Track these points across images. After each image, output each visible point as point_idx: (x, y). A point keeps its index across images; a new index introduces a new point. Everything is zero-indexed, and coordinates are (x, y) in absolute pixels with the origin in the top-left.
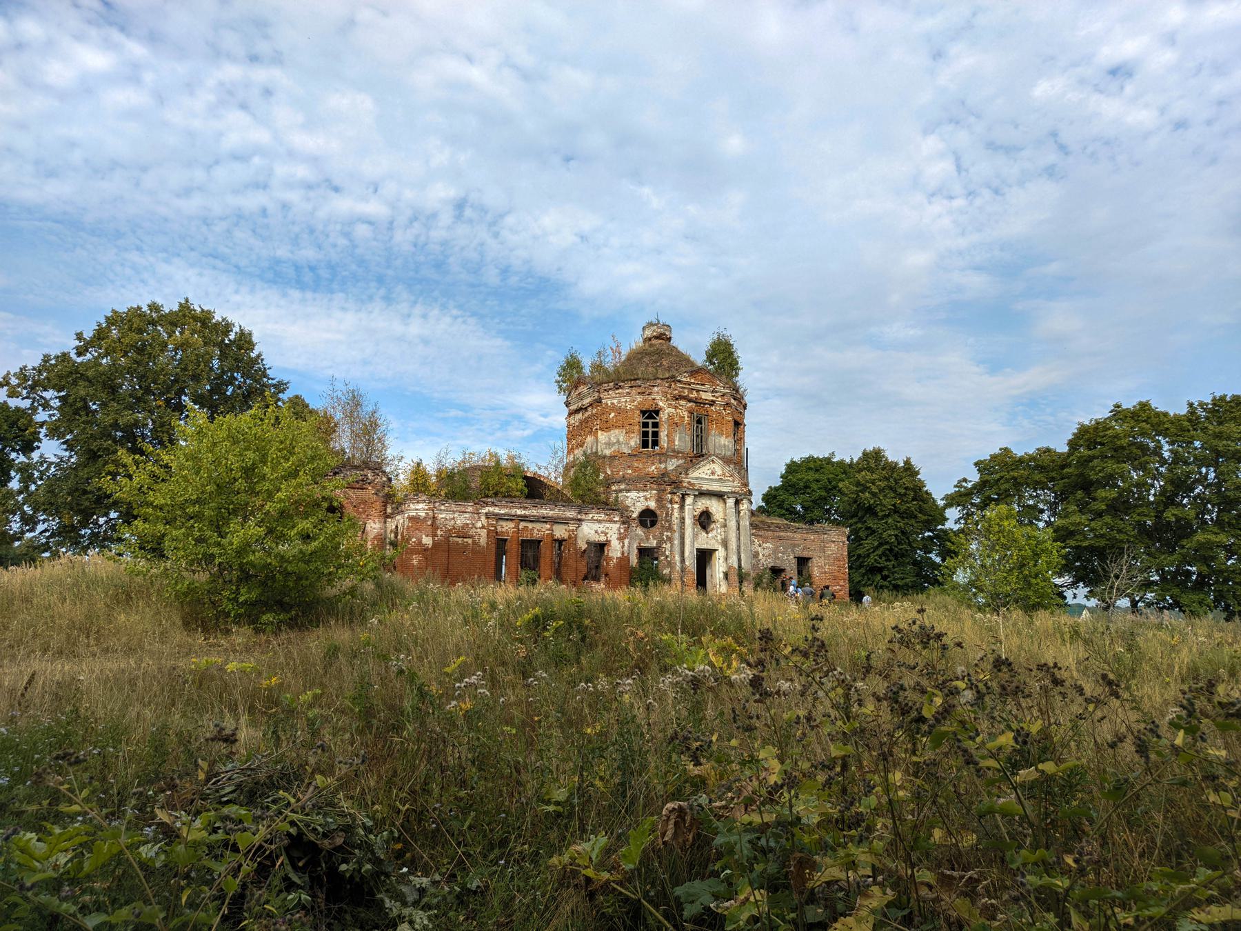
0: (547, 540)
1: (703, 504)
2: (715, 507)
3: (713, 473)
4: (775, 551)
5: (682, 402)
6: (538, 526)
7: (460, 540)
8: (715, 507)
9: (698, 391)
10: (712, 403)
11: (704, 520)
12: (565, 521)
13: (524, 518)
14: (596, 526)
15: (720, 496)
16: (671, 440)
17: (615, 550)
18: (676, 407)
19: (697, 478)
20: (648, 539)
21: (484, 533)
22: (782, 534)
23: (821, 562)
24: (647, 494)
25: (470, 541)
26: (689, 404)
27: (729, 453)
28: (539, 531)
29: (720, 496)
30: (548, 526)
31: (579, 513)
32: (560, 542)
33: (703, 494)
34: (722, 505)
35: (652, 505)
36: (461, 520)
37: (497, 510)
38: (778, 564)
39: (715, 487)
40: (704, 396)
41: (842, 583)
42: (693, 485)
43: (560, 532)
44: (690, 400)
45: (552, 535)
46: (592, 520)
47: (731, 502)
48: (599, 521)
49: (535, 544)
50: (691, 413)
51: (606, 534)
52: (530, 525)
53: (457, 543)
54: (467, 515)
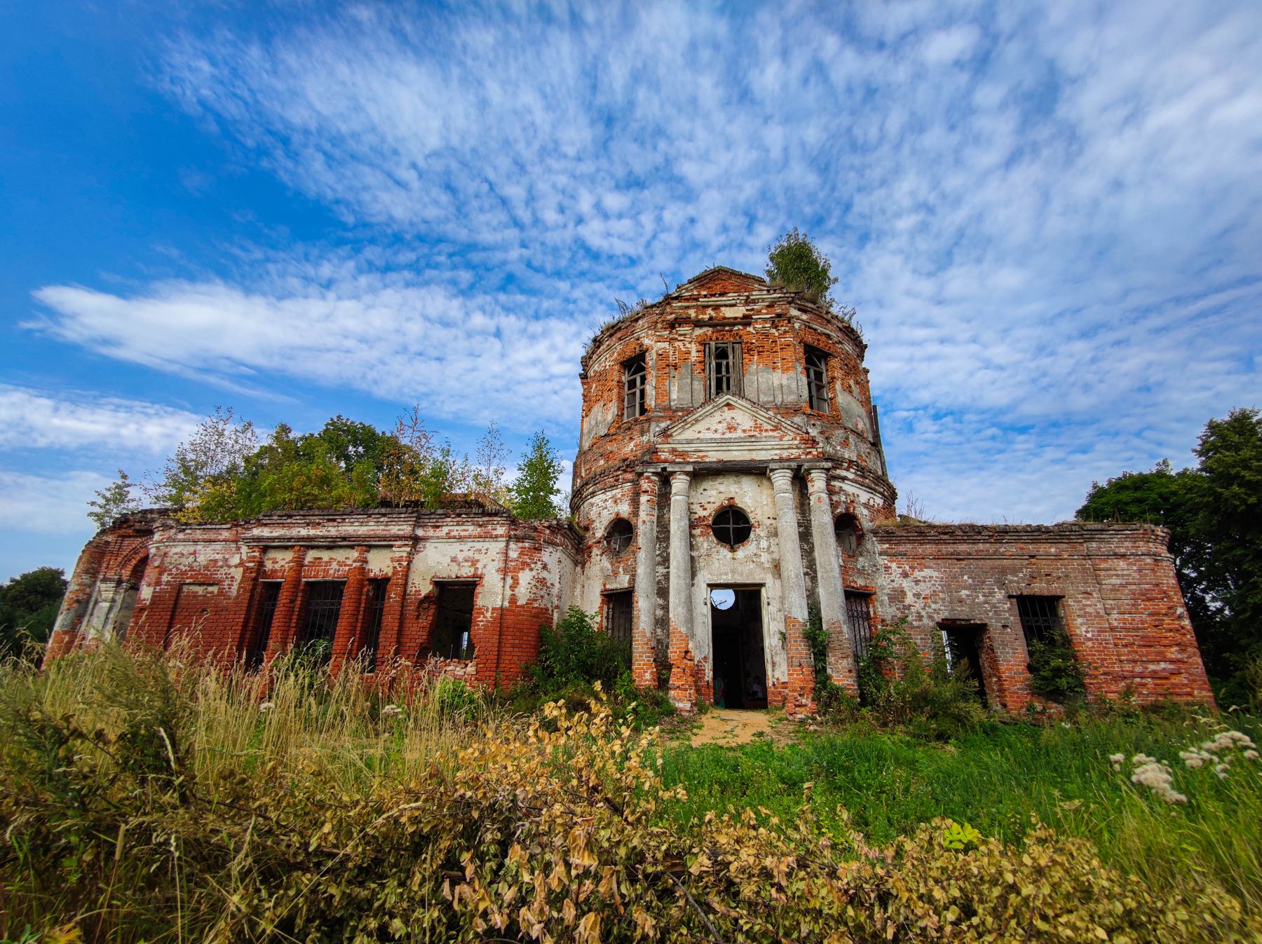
0: (352, 581)
1: (715, 494)
2: (747, 494)
3: (731, 428)
4: (950, 586)
5: (685, 329)
6: (340, 555)
7: (200, 590)
8: (747, 494)
9: (716, 308)
10: (746, 320)
11: (732, 527)
12: (385, 543)
13: (310, 544)
14: (454, 549)
15: (759, 471)
16: (662, 393)
17: (492, 596)
18: (671, 341)
19: (689, 442)
20: (616, 574)
21: (238, 574)
22: (963, 548)
23: (1094, 605)
25: (215, 589)
26: (698, 331)
27: (791, 398)
28: (338, 563)
29: (759, 471)
30: (355, 554)
31: (417, 524)
32: (381, 584)
33: (702, 474)
35: (624, 509)
36: (206, 554)
37: (266, 532)
38: (962, 612)
39: (738, 455)
40: (729, 313)
41: (1173, 653)
42: (683, 454)
43: (380, 563)
44: (698, 324)
45: (362, 570)
46: (449, 536)
47: (782, 479)
48: (461, 539)
49: (334, 589)
50: (703, 343)
51: (474, 563)
52: (325, 555)
53: (195, 595)
54: (218, 546)
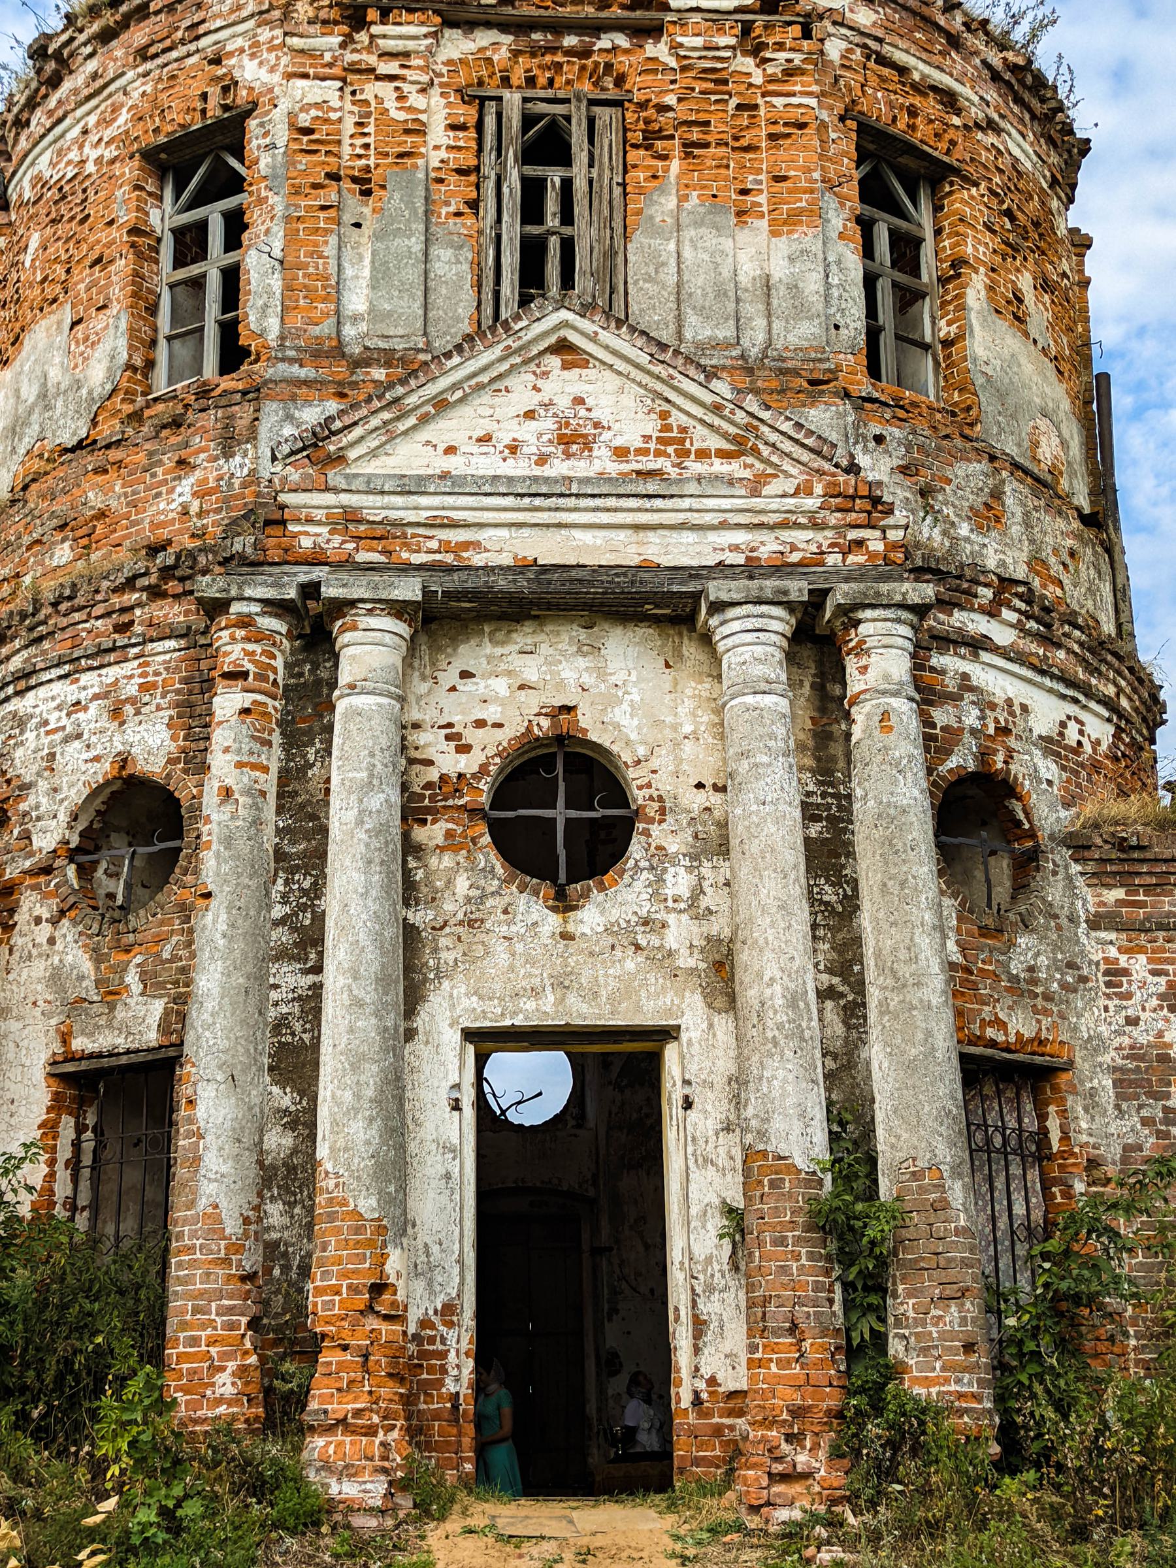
1: (502, 692)
2: (623, 695)
3: (572, 440)
8: (623, 695)
11: (562, 815)
15: (667, 609)
16: (311, 287)
19: (410, 486)
20: (111, 993)
24: (123, 675)
29: (667, 609)
33: (457, 612)
34: (694, 688)
35: (151, 743)
42: (386, 533)
47: (752, 643)
